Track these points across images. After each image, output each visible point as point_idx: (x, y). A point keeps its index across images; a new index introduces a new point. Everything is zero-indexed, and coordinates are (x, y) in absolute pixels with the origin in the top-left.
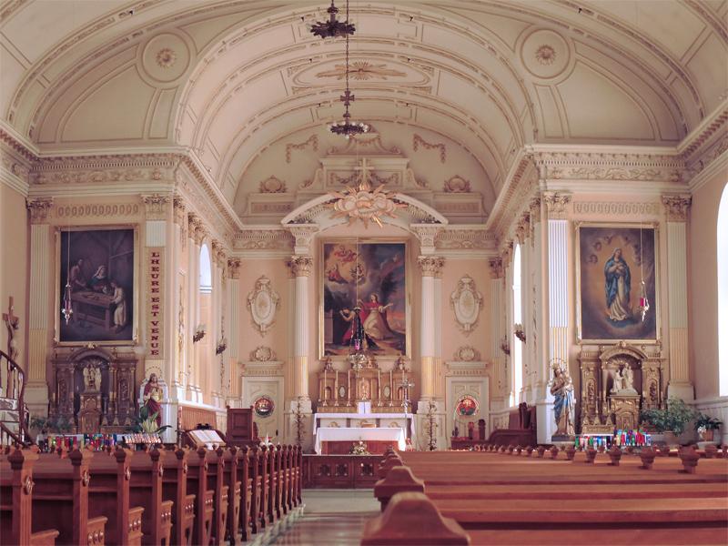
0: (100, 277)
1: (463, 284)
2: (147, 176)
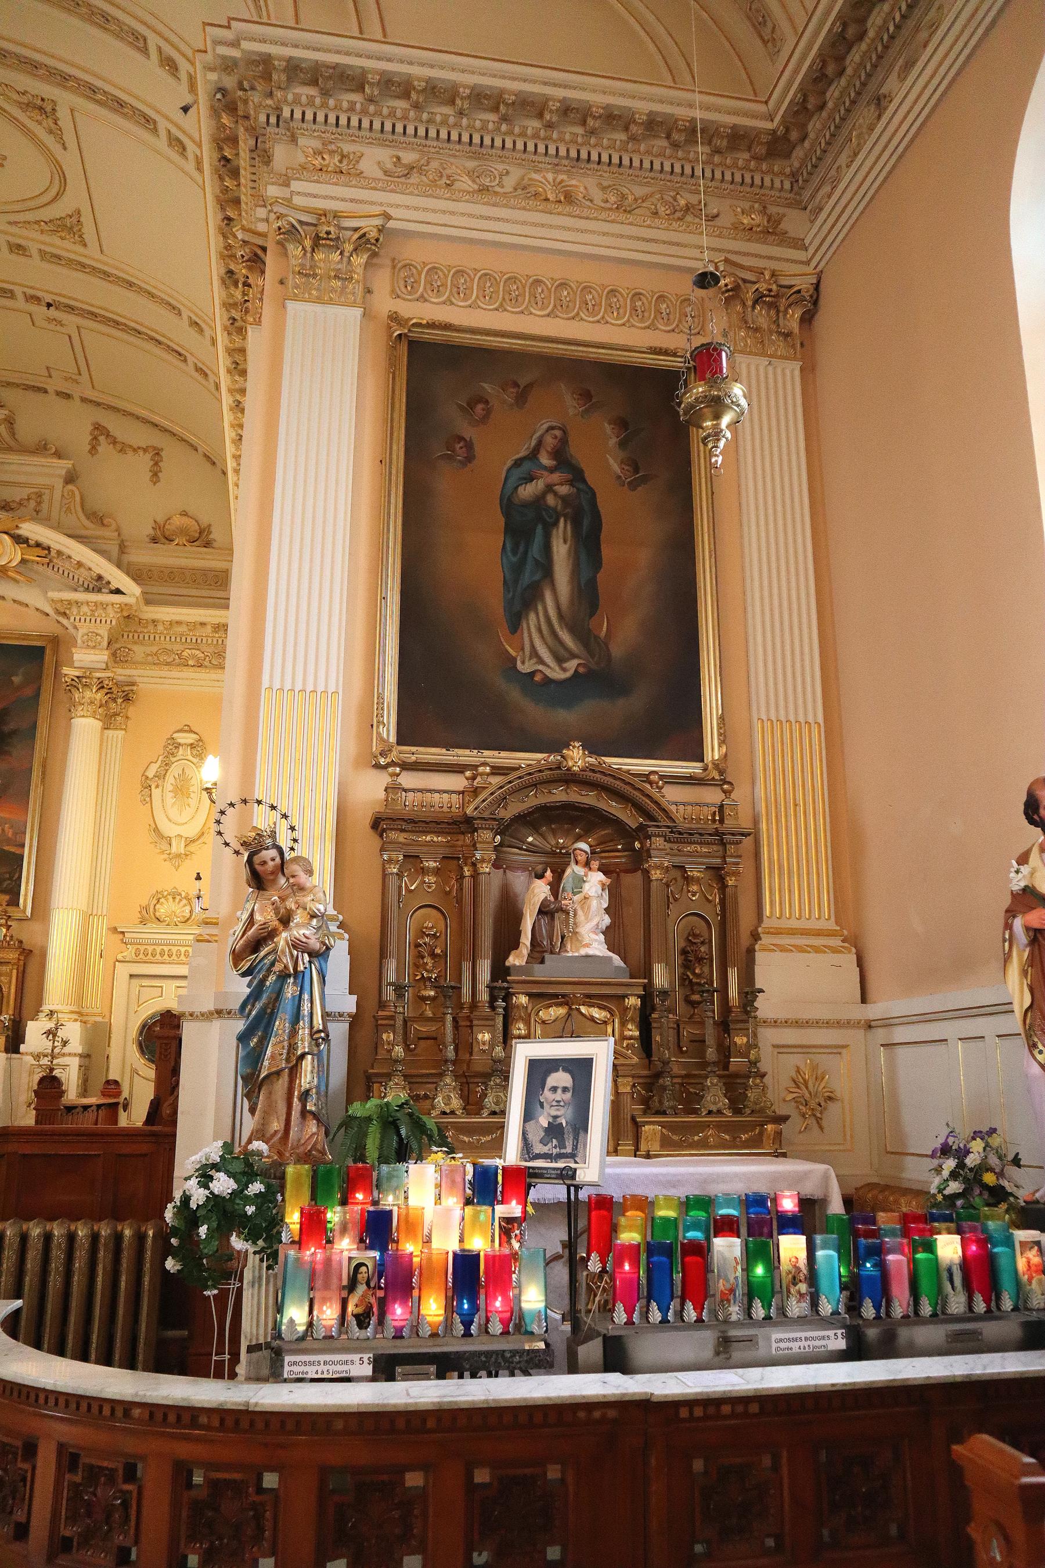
1: (178, 746)
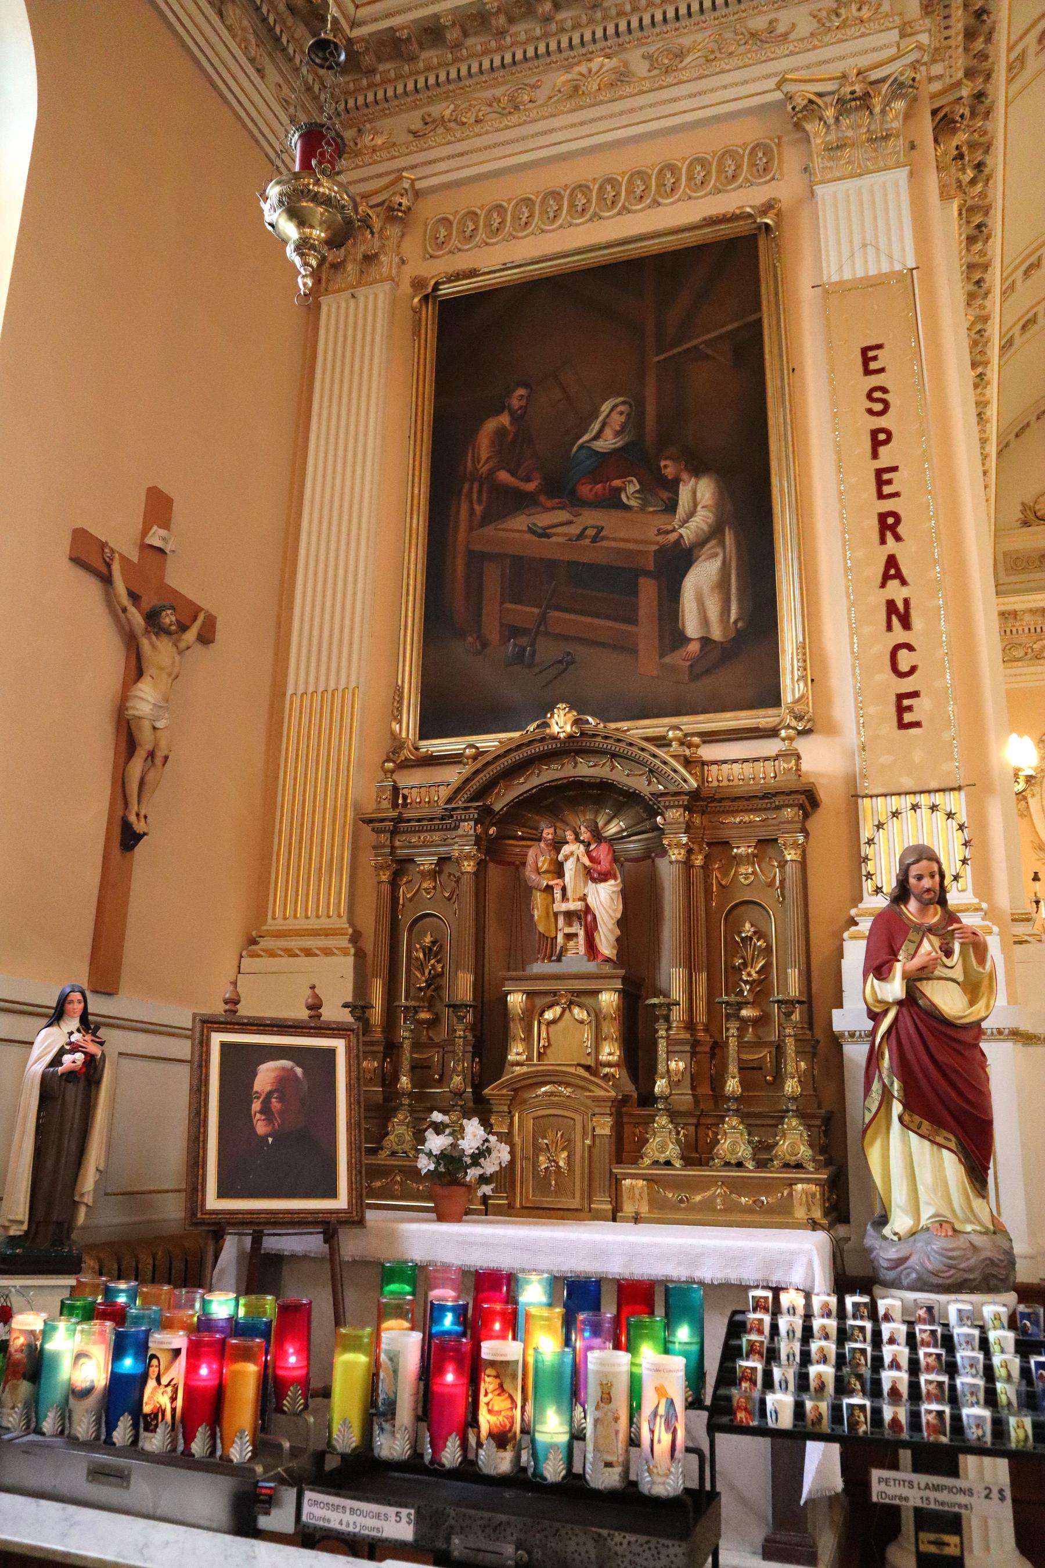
0: (608, 443)
2: (806, 26)
